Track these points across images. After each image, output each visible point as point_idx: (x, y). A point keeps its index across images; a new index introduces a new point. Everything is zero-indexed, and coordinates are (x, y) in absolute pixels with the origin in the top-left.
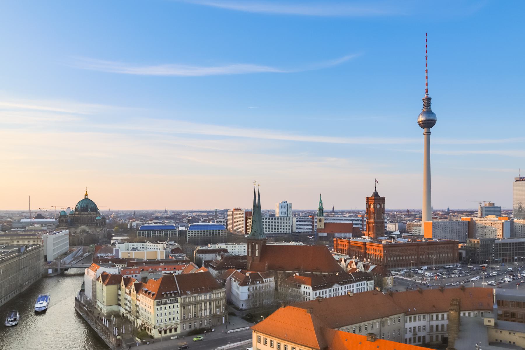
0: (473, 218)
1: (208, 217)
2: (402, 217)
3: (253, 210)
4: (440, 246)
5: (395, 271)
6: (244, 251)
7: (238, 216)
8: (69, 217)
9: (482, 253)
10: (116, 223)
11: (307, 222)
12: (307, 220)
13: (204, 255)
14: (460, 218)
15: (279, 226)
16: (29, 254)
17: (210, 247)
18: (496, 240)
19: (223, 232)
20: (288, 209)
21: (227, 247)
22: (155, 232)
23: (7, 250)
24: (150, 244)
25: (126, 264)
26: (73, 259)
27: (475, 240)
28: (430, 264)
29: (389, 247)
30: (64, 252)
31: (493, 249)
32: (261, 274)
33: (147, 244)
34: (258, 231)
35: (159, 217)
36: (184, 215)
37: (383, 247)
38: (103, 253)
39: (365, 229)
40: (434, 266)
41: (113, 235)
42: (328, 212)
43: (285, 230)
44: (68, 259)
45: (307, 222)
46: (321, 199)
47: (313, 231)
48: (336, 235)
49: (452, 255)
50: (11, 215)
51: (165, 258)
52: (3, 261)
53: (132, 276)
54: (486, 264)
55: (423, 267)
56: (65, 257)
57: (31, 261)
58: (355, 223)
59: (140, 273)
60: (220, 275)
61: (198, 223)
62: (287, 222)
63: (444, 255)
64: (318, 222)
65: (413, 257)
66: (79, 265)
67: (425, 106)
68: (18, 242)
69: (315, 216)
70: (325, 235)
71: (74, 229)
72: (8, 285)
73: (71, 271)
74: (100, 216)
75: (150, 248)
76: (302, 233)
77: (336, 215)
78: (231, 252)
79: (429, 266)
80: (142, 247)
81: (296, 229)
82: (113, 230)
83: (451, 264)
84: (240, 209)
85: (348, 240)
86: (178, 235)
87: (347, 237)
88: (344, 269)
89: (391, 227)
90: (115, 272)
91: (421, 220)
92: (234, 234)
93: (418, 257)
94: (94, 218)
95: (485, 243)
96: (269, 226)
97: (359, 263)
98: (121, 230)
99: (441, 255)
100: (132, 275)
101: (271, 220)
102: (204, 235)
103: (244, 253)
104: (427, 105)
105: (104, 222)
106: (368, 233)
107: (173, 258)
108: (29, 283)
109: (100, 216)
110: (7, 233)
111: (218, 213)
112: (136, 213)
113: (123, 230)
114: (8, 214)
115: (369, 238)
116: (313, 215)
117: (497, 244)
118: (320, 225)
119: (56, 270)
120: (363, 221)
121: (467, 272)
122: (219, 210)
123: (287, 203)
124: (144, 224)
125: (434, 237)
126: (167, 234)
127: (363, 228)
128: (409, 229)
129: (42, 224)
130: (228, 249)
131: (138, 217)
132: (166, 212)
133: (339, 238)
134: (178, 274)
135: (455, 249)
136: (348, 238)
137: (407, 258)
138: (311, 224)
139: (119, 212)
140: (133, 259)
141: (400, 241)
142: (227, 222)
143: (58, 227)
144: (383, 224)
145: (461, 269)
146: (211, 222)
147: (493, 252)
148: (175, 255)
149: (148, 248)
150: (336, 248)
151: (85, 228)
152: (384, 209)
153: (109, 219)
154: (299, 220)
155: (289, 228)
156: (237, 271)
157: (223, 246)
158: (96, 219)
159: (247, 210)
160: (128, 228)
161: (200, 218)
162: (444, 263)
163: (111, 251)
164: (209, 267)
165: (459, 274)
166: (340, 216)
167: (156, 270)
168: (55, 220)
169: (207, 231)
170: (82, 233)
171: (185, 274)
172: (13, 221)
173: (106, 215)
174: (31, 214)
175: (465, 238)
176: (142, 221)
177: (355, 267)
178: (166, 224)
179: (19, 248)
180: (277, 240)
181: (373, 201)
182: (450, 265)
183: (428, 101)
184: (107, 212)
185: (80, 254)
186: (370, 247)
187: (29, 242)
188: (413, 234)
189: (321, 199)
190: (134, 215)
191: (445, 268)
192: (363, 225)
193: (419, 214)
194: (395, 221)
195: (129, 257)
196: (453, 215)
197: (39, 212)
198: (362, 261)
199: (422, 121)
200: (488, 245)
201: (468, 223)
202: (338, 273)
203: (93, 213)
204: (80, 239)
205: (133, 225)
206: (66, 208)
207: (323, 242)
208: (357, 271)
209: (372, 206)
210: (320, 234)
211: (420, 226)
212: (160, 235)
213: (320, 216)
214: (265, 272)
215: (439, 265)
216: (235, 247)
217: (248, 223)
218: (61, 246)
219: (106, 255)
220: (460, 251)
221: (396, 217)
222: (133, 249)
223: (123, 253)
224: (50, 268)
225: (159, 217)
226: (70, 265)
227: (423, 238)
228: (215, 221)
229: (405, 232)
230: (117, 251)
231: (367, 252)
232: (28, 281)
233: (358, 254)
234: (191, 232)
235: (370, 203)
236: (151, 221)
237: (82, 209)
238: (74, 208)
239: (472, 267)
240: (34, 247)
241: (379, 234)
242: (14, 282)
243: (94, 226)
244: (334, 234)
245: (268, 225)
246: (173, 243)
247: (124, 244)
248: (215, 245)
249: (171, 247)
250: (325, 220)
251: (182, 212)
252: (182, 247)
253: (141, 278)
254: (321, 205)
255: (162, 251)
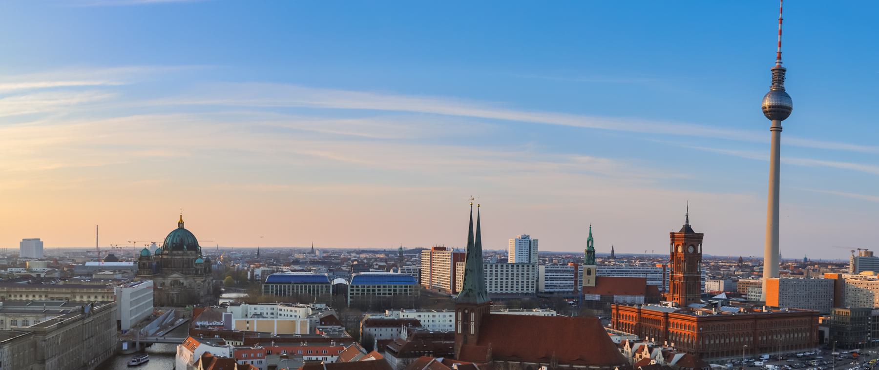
0: (841, 275)
1: (386, 261)
2: (731, 269)
3: (468, 250)
4: (791, 320)
5: (717, 363)
6: (451, 318)
7: (441, 261)
8: (155, 259)
9: (853, 332)
10: (227, 269)
11: (565, 275)
12: (565, 271)
13: (377, 329)
14: (823, 274)
15: (515, 281)
16: (95, 317)
17: (388, 315)
18: (872, 311)
19: (413, 288)
20: (532, 250)
21: (419, 316)
22: (293, 286)
23: (67, 308)
24: (283, 308)
25: (242, 341)
26: (158, 328)
27: (844, 311)
28: (775, 351)
29: (707, 321)
30: (145, 316)
31: (869, 324)
32: (479, 367)
33: (279, 307)
34: (475, 288)
35: (301, 261)
36: (343, 257)
37: (697, 321)
38: (206, 321)
39: (668, 289)
40: (780, 353)
41: (223, 289)
42: (603, 257)
43: (525, 288)
44: (151, 328)
45: (565, 275)
46: (590, 234)
47: (576, 291)
48: (616, 298)
49: (808, 334)
50: (73, 256)
51: (308, 333)
52: (62, 326)
53: (252, 362)
54: (859, 350)
55: (763, 356)
56: (147, 325)
57: (99, 327)
58: (651, 278)
59: (266, 357)
60: (405, 366)
61: (369, 272)
62: (528, 274)
63: (796, 335)
64: (585, 275)
65: (747, 339)
66: (169, 338)
67: (775, 82)
68: (82, 297)
69: (580, 264)
70: (597, 297)
71: (161, 278)
72: (68, 363)
73: (156, 348)
74: (202, 258)
75: (283, 315)
76: (556, 294)
77: (617, 263)
78: (426, 326)
79: (773, 354)
80: (269, 311)
81: (546, 286)
82: (223, 281)
83: (807, 351)
84: (444, 249)
85: (637, 307)
86: (333, 293)
87: (636, 302)
88: (630, 360)
89: (711, 286)
90: (224, 354)
91: (761, 276)
92: (432, 293)
93: (755, 339)
94: (192, 260)
95: (854, 316)
96: (506, 284)
97: (655, 350)
98: (236, 282)
99: (792, 336)
100: (252, 360)
101: (499, 270)
102: (378, 294)
103: (450, 328)
104: (779, 80)
105: (208, 268)
106: (673, 296)
107: (322, 334)
108: (96, 362)
109: (202, 258)
110: (68, 283)
111: (404, 255)
112: (261, 253)
113: (238, 282)
114: (68, 253)
115: (674, 305)
116: (576, 261)
117: (874, 317)
118: (589, 281)
119: (134, 344)
120: (664, 274)
121: (831, 362)
122: (406, 249)
123: (530, 238)
124: (275, 272)
125: (782, 303)
126: (314, 290)
127: (664, 288)
128: (741, 290)
129: (115, 269)
130: (422, 319)
131: (264, 259)
132: (313, 251)
133: (622, 304)
134: (330, 362)
135: (814, 325)
136: (637, 304)
137: (737, 340)
138: (572, 278)
139: (234, 251)
140: (254, 333)
141: (727, 310)
142: (420, 270)
143: (137, 274)
144: (698, 280)
145: (821, 357)
146: (392, 270)
147: (869, 330)
148: (327, 328)
149: (280, 315)
150: (615, 322)
151: (178, 277)
152: (701, 254)
153: (216, 263)
154: (550, 270)
155: (532, 284)
156: (435, 360)
157: (412, 315)
158: (196, 262)
159: (457, 250)
160: (248, 279)
161: (372, 263)
162: (796, 349)
163: (219, 318)
164: (386, 352)
165: (819, 365)
166: (625, 265)
167: (292, 354)
168: (134, 263)
169: (384, 287)
170: (174, 286)
171: (343, 363)
172: (75, 264)
173: (212, 256)
174: (99, 254)
175: (829, 306)
176: (271, 267)
177: (648, 356)
178: (311, 273)
179: (82, 307)
180: (510, 307)
181: (682, 240)
182: (805, 351)
183: (780, 74)
184: (214, 251)
185: (170, 321)
186: (676, 321)
187: (96, 297)
188: (749, 298)
189: (590, 234)
190: (258, 257)
191: (798, 357)
192: (664, 281)
193: (759, 265)
194: (719, 277)
195: (248, 328)
196: (812, 268)
197: (111, 251)
198: (661, 346)
199: (769, 107)
200: (861, 318)
201: (834, 282)
202: (619, 366)
203: (191, 253)
204: (171, 295)
205: (255, 274)
206: (150, 245)
207: (592, 310)
208: (652, 364)
209: (680, 249)
210: (588, 297)
211: (759, 286)
212: (301, 292)
213: (589, 264)
214: (487, 364)
215: (788, 353)
216: (434, 316)
217: (458, 274)
218: (136, 308)
219: (211, 324)
220: (821, 328)
221: (722, 269)
222: (255, 315)
223: (239, 321)
224: (125, 342)
225: (301, 261)
226: (155, 338)
227: (764, 307)
228: (399, 268)
229: (734, 296)
230: (229, 318)
231: (669, 329)
232: (94, 359)
233: (654, 332)
234: (355, 288)
235: (677, 243)
236: (287, 267)
237: (174, 245)
238: (162, 245)
239: (838, 353)
240: (103, 305)
241: (691, 299)
242: (75, 359)
243: (193, 274)
244: (613, 298)
245: (494, 278)
246: (323, 306)
247: (241, 306)
248: (397, 312)
249: (320, 313)
250: (598, 271)
251: (340, 252)
252: (339, 315)
253: (267, 366)
254: (590, 244)
255: (303, 320)
